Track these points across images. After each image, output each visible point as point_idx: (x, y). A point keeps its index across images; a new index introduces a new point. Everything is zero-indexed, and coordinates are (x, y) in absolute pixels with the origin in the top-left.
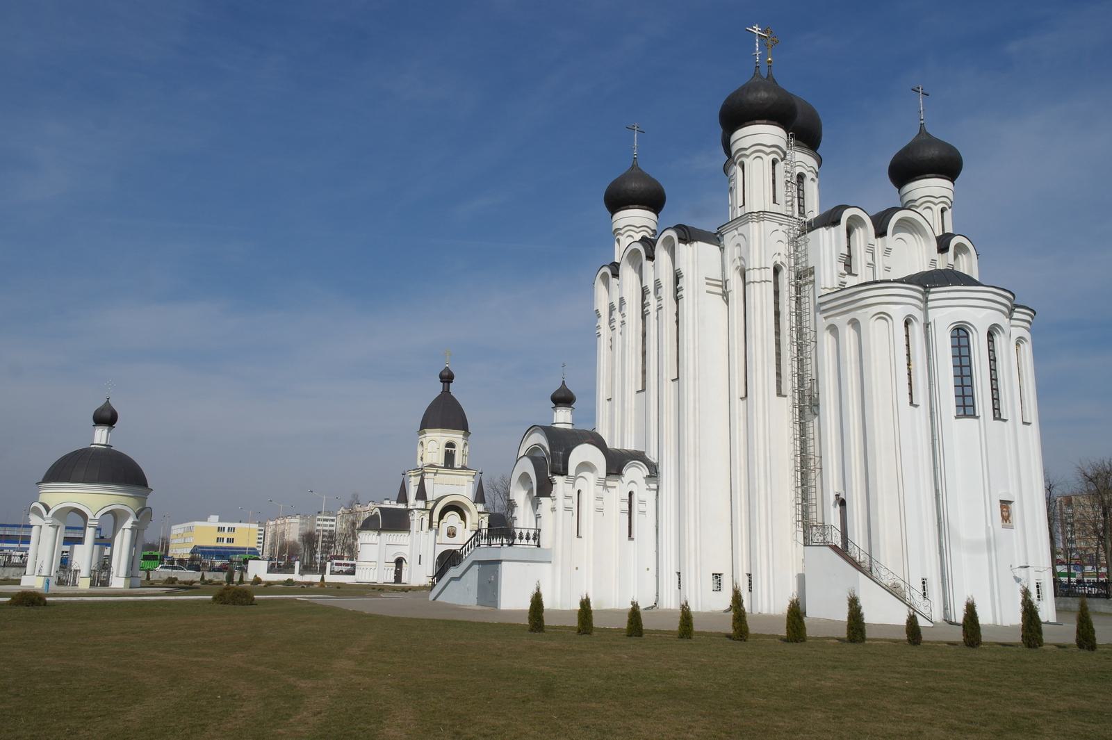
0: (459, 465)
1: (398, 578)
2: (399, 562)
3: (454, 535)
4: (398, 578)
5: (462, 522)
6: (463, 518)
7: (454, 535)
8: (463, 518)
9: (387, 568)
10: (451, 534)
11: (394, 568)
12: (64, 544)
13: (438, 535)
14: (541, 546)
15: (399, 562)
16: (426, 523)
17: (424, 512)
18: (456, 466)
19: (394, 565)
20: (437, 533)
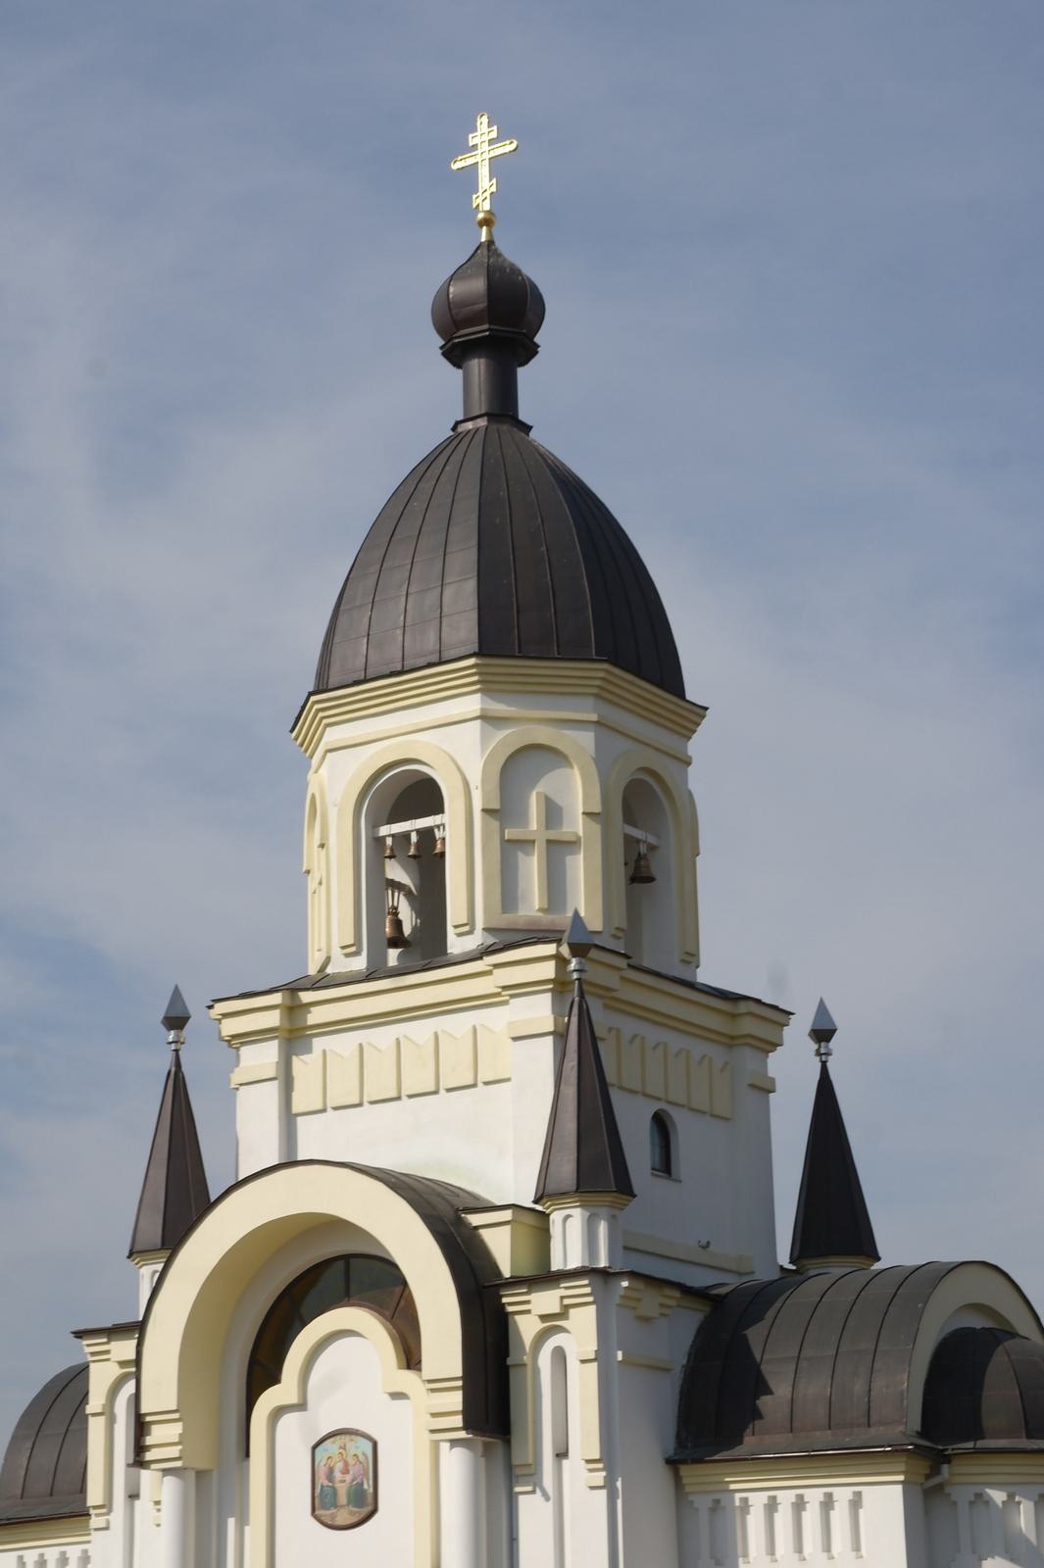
3: (322, 1504)
7: (364, 1506)
18: (456, 945)
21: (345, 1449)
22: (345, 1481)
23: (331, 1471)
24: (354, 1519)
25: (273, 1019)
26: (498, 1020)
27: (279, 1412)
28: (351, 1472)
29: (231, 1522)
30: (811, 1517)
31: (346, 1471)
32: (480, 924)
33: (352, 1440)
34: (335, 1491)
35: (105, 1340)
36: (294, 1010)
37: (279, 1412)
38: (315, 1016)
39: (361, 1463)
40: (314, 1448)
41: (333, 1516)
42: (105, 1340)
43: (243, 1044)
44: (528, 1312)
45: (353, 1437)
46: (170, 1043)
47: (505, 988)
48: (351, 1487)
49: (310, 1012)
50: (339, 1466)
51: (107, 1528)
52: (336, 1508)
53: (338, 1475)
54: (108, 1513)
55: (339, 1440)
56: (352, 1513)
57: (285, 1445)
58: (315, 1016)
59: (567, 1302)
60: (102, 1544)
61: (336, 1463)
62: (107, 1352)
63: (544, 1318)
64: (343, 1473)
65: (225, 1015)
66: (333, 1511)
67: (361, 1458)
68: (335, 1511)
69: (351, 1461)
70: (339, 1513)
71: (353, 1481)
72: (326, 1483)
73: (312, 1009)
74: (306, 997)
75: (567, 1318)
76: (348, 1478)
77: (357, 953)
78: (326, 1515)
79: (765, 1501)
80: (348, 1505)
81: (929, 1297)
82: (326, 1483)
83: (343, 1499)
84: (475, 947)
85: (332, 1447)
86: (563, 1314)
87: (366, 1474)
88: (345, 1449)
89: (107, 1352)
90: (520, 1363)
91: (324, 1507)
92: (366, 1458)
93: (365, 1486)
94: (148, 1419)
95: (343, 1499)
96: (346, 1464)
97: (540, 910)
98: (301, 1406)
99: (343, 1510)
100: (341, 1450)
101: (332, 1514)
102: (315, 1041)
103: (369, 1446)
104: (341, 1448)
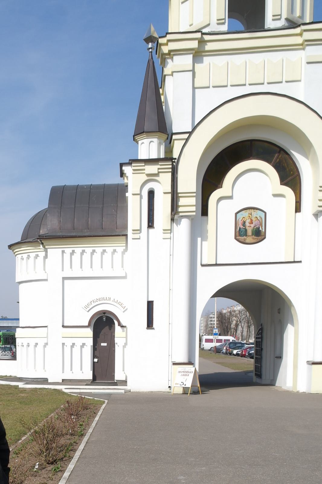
0: (277, 17)
1: (103, 367)
2: (103, 325)
3: (259, 235)
4: (103, 367)
5: (288, 191)
6: (290, 176)
7: (259, 235)
8: (290, 176)
9: (69, 342)
10: (251, 231)
11: (90, 342)
12: (205, 339)
13: (173, 211)
14: (263, 376)
15: (103, 325)
16: (163, 204)
17: (152, 169)
18: (269, 23)
19: (89, 332)
20: (197, 232)
21: (251, 215)
22: (251, 227)
23: (244, 222)
24: (255, 241)
25: (194, 45)
26: (301, 56)
27: (220, 199)
28: (254, 223)
29: (199, 239)
30: (67, 256)
31: (251, 222)
32: (284, 15)
33: (255, 211)
34: (246, 230)
35: (144, 164)
36: (202, 42)
37: (220, 199)
38: (209, 47)
39: (258, 220)
40: (236, 214)
41: (245, 240)
42: (144, 164)
43: (174, 55)
44: (144, 173)
45: (255, 210)
46: (149, 48)
47: (307, 41)
48: (254, 229)
49: (207, 45)
50: (248, 221)
51: (139, 239)
52: (246, 236)
53: (247, 224)
54: (139, 233)
55: (248, 211)
56: (253, 239)
57: (224, 209)
58: (209, 47)
59: (159, 171)
60: (136, 245)
61: (247, 220)
62: (144, 170)
63: (148, 175)
64: (250, 224)
65: (169, 41)
66: (245, 237)
67: (259, 218)
68: (246, 237)
69: (254, 219)
70: (247, 238)
71: (255, 227)
72: (242, 227)
73: (207, 43)
74: (206, 38)
75: (159, 176)
76: (252, 226)
77: (224, 23)
78: (241, 239)
79: (71, 252)
80: (252, 235)
81: (291, 180)
82: (242, 227)
83: (249, 232)
84: (281, 26)
85: (245, 214)
86: (157, 175)
87: (261, 224)
88: (251, 215)
89: (144, 170)
90: (77, 186)
91: (240, 235)
92: (261, 218)
93: (261, 229)
94: (180, 195)
95: (249, 232)
96: (252, 220)
97: (298, 17)
98: (231, 198)
99: (249, 237)
100: (250, 215)
101: (244, 238)
102: (205, 58)
103: (263, 215)
104: (249, 214)
